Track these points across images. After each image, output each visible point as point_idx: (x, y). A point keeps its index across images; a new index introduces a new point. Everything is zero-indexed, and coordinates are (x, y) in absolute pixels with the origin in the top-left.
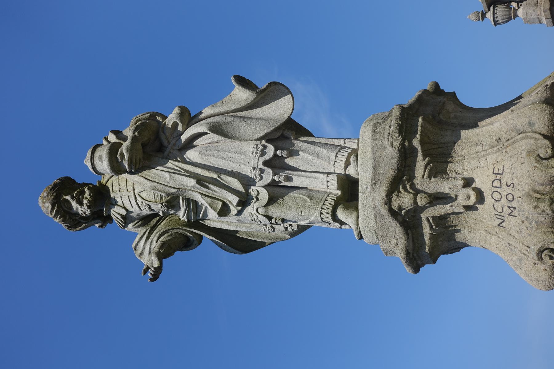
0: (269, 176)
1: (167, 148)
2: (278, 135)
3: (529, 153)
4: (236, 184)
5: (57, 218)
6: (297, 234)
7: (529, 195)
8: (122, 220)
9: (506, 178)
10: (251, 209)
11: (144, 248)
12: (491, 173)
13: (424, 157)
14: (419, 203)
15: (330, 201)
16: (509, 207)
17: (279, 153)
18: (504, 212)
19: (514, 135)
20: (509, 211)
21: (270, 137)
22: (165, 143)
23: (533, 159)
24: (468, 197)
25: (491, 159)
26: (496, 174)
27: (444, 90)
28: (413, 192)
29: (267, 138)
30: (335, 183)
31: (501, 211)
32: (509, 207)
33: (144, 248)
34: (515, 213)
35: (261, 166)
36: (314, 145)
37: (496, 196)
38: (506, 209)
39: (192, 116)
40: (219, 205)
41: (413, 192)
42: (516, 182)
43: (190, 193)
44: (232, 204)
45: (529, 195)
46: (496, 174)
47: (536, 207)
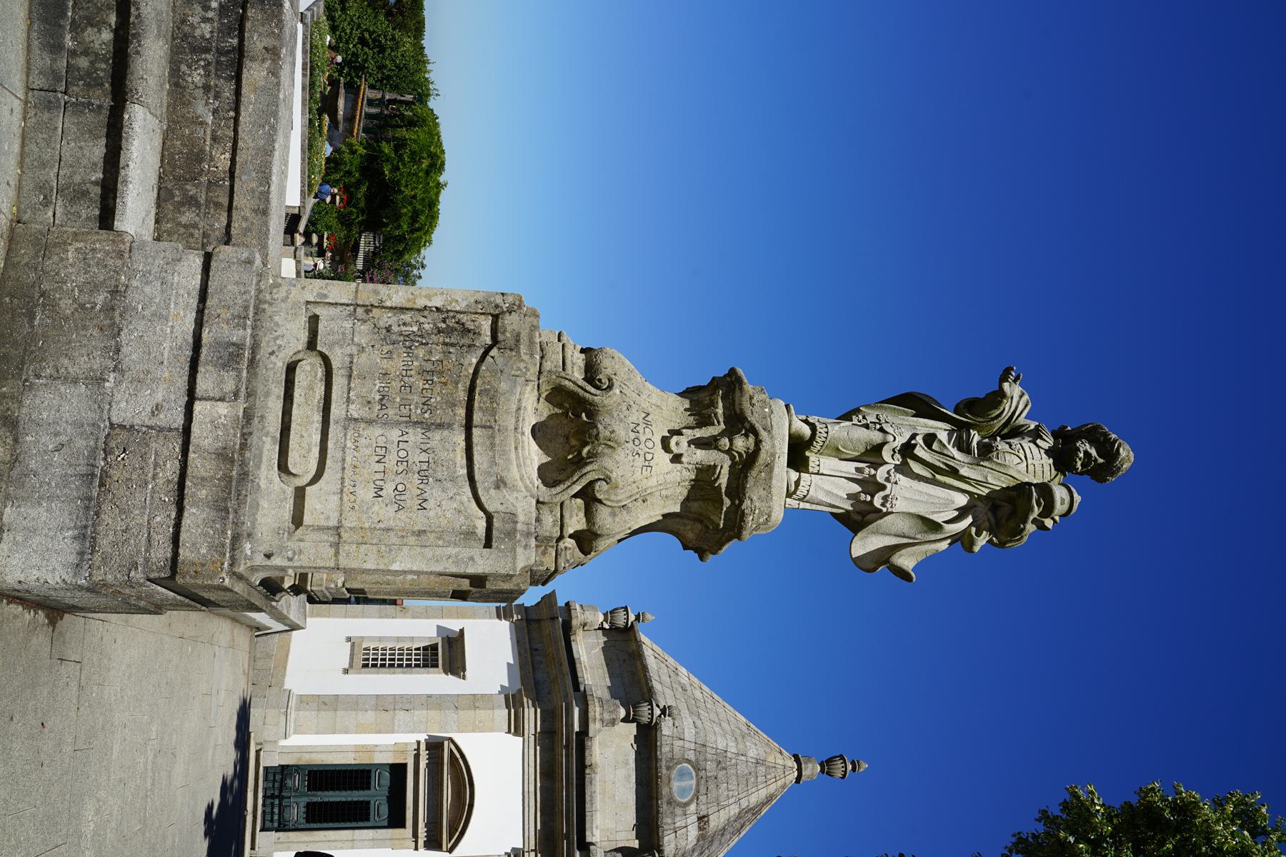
4: (916, 468)
7: (619, 444)
33: (1018, 403)
34: (632, 426)
35: (889, 485)
40: (935, 446)
42: (630, 458)
47: (613, 432)
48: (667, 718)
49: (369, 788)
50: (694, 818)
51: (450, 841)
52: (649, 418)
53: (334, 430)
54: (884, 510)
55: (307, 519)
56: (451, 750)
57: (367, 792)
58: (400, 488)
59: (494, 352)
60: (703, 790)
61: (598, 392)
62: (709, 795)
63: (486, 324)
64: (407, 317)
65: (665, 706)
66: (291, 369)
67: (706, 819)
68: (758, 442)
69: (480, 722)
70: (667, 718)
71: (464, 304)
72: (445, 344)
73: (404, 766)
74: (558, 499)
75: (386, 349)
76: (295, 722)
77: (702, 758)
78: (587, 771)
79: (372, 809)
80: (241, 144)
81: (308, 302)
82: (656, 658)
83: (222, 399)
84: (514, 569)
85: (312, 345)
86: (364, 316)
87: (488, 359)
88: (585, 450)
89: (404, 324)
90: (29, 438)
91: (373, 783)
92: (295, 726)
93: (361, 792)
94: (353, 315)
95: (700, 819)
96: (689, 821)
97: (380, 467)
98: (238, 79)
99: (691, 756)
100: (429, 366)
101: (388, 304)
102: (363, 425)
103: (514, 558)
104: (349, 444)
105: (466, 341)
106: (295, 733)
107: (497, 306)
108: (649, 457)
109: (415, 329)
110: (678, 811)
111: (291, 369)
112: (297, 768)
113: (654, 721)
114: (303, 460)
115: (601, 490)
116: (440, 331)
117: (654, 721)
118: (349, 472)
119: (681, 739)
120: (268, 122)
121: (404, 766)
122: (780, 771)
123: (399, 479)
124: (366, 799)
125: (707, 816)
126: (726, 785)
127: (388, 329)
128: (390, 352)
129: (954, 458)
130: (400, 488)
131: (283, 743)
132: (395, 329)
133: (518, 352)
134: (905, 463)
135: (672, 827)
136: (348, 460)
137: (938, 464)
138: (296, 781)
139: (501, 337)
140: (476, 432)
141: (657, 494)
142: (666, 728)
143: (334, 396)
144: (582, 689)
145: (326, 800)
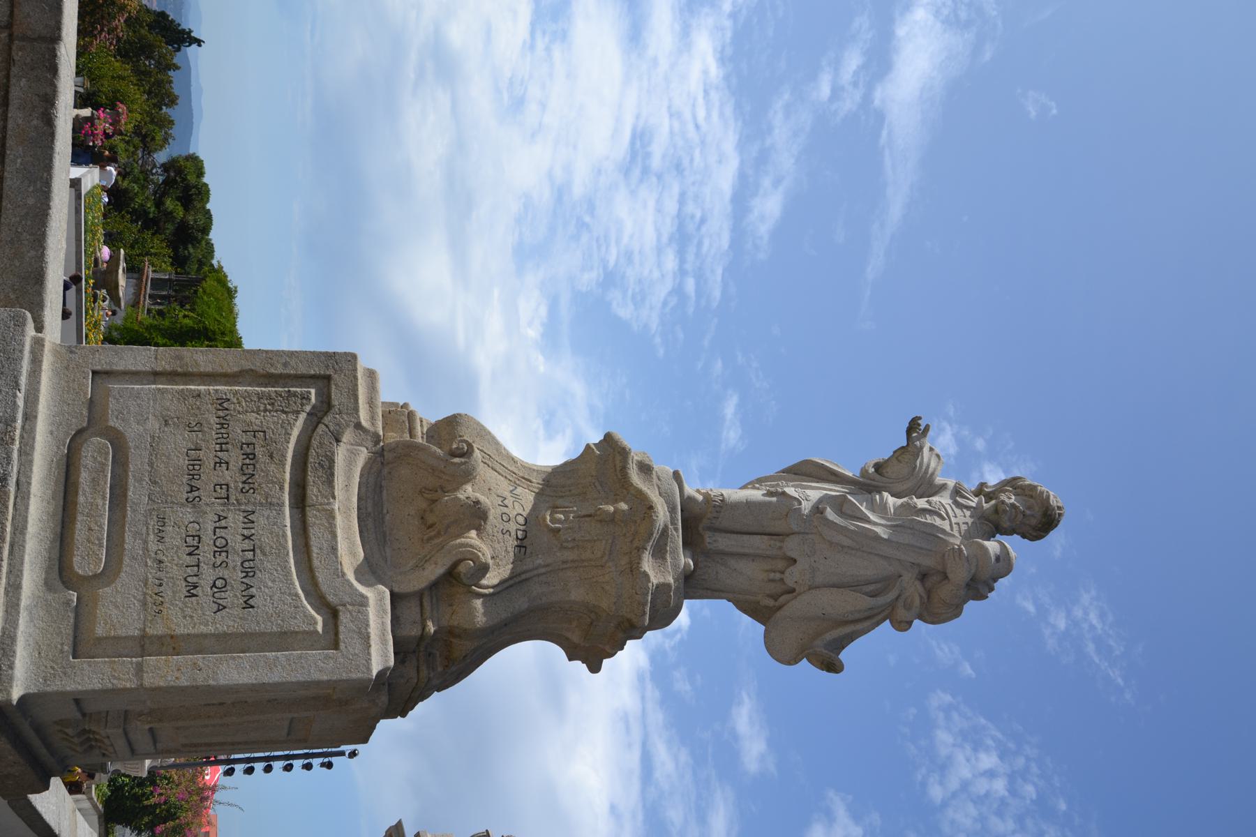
1: (916, 578)
2: (782, 599)
8: (873, 528)
12: (528, 547)
14: (974, 505)
16: (506, 506)
18: (511, 501)
20: (506, 502)
21: (791, 595)
22: (918, 583)
26: (523, 547)
27: (48, 789)
28: (883, 522)
29: (794, 594)
31: (515, 503)
32: (506, 506)
36: (991, 589)
38: (510, 505)
39: (888, 621)
41: (883, 522)
46: (523, 547)
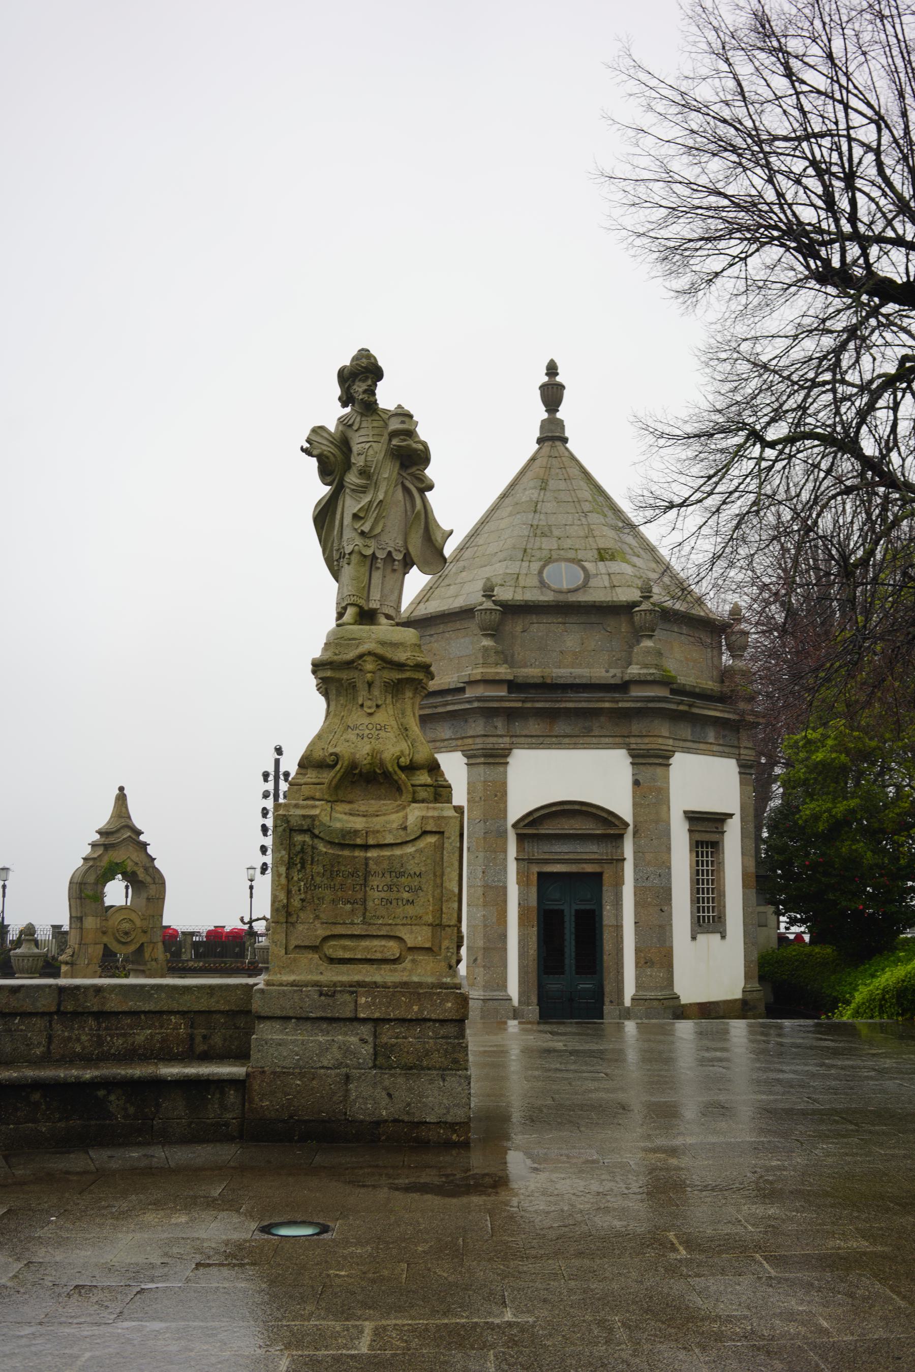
0: (381, 555)
3: (402, 752)
4: (378, 530)
5: (760, 1092)
6: (502, 856)
7: (374, 749)
9: (382, 733)
10: (359, 541)
11: (322, 436)
13: (398, 680)
15: (362, 602)
17: (396, 563)
19: (364, 661)
23: (398, 754)
24: (370, 708)
25: (394, 723)
30: (374, 606)
33: (322, 436)
34: (359, 739)
35: (389, 549)
37: (370, 726)
40: (362, 515)
42: (381, 740)
43: (372, 492)
44: (362, 525)
45: (374, 749)
47: (368, 754)
48: (495, 593)
49: (562, 911)
50: (601, 564)
51: (616, 826)
52: (352, 726)
53: (373, 931)
54: (405, 551)
55: (428, 945)
56: (525, 826)
57: (566, 913)
58: (407, 889)
59: (316, 832)
60: (571, 555)
61: (340, 763)
62: (577, 547)
63: (299, 838)
64: (294, 889)
65: (483, 596)
66: (332, 961)
67: (602, 551)
68: (370, 653)
69: (496, 796)
70: (495, 593)
71: (283, 852)
72: (312, 864)
73: (540, 875)
74: (411, 789)
75: (316, 901)
76: (495, 991)
77: (538, 554)
78: (549, 681)
79: (583, 907)
80: (165, 1009)
81: (286, 953)
82: (428, 600)
83: (356, 1001)
84: (456, 817)
85: (314, 949)
86: (295, 916)
87: (321, 835)
88: (378, 771)
89: (300, 890)
90: (384, 1113)
91: (556, 907)
92: (498, 990)
93: (567, 919)
94: (293, 924)
95: (602, 559)
96: (603, 571)
97: (394, 902)
98: (117, 1013)
99: (536, 566)
100: (328, 873)
101: (285, 901)
102: (367, 914)
103: (450, 817)
104: (380, 922)
105: (309, 850)
106: (506, 991)
107: (284, 830)
108: (378, 727)
109: (302, 884)
110: (593, 583)
111: (332, 961)
112: (540, 987)
113: (498, 608)
114: (392, 949)
115: (404, 761)
116: (303, 867)
117: (498, 608)
118: (398, 921)
119: (518, 578)
120: (148, 991)
121: (540, 875)
122: (554, 462)
123: (402, 890)
124: (573, 913)
125: (599, 550)
126: (567, 527)
127: (303, 900)
128: (318, 899)
129: (370, 502)
130: (407, 889)
131: (515, 1002)
132: (303, 896)
133: (316, 816)
134: (375, 536)
135: (609, 590)
136: (390, 922)
137: (375, 515)
138: (555, 985)
139: (305, 827)
140: (371, 842)
141: (402, 720)
142: (505, 594)
143: (349, 933)
144: (462, 685)
145: (573, 954)
